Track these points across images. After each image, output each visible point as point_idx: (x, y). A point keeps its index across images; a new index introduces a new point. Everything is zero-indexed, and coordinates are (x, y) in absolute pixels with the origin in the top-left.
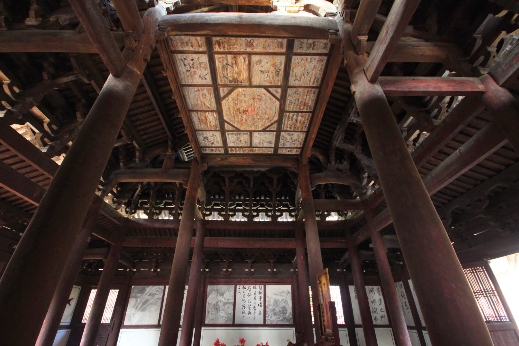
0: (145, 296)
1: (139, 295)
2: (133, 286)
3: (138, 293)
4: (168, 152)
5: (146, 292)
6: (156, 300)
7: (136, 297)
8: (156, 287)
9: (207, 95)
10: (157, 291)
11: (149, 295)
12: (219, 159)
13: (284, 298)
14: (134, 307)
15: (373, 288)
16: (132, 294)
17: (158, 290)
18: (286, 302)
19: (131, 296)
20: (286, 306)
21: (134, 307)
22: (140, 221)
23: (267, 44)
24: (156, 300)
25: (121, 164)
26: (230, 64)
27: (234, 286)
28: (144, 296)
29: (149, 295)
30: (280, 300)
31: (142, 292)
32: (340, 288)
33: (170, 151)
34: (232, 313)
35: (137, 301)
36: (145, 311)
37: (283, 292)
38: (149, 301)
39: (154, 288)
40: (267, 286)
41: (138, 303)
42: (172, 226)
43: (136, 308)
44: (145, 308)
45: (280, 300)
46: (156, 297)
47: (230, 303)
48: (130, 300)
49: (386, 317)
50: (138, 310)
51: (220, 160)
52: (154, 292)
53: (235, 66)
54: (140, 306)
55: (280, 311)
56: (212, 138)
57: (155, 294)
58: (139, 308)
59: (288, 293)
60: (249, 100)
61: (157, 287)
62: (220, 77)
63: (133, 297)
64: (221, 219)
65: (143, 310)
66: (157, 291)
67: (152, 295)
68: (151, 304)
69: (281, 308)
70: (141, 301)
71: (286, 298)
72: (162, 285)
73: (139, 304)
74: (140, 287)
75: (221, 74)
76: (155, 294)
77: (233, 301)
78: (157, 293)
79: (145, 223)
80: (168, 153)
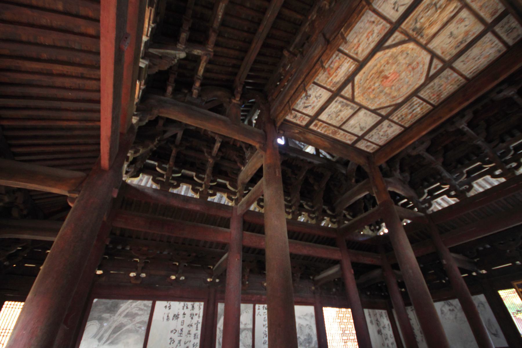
0: (118, 318)
1: (106, 315)
2: (95, 300)
3: (105, 312)
4: (235, 99)
5: (121, 310)
6: (139, 325)
7: (100, 319)
8: (139, 302)
9: (374, 35)
10: (141, 309)
11: (126, 316)
12: (297, 131)
13: (308, 323)
14: (95, 336)
15: (381, 313)
16: (94, 313)
17: (143, 307)
18: (310, 328)
19: (90, 317)
20: (311, 333)
21: (95, 336)
22: (146, 191)
23: (486, 5)
24: (139, 325)
25: (170, 89)
26: (438, 6)
27: (251, 306)
28: (116, 317)
29: (126, 316)
30: (305, 325)
31: (113, 310)
32: (9, 300)
33: (238, 99)
34: (251, 344)
35: (102, 326)
36: (117, 343)
37: (306, 315)
38: (125, 326)
39: (134, 304)
40: (257, 306)
41: (103, 329)
42: (198, 208)
43: (100, 340)
44: (116, 339)
45: (305, 325)
46: (138, 319)
47: (247, 329)
48: (88, 324)
49: (395, 344)
50: (103, 342)
51: (297, 133)
52: (135, 311)
53: (439, 11)
54: (107, 335)
55: (305, 340)
56: (315, 99)
57: (137, 314)
58: (105, 339)
59: (312, 316)
60: (403, 65)
61: (139, 303)
62: (413, 16)
63: (95, 319)
64: (452, 201)
65: (112, 343)
66: (141, 309)
67: (131, 316)
68: (129, 331)
69: (306, 335)
70: (110, 327)
71: (310, 322)
72: (148, 299)
73: (106, 331)
74: (109, 302)
75: (419, 12)
76: (137, 314)
77: (251, 326)
78: (140, 312)
79: (155, 195)
80: (234, 101)
